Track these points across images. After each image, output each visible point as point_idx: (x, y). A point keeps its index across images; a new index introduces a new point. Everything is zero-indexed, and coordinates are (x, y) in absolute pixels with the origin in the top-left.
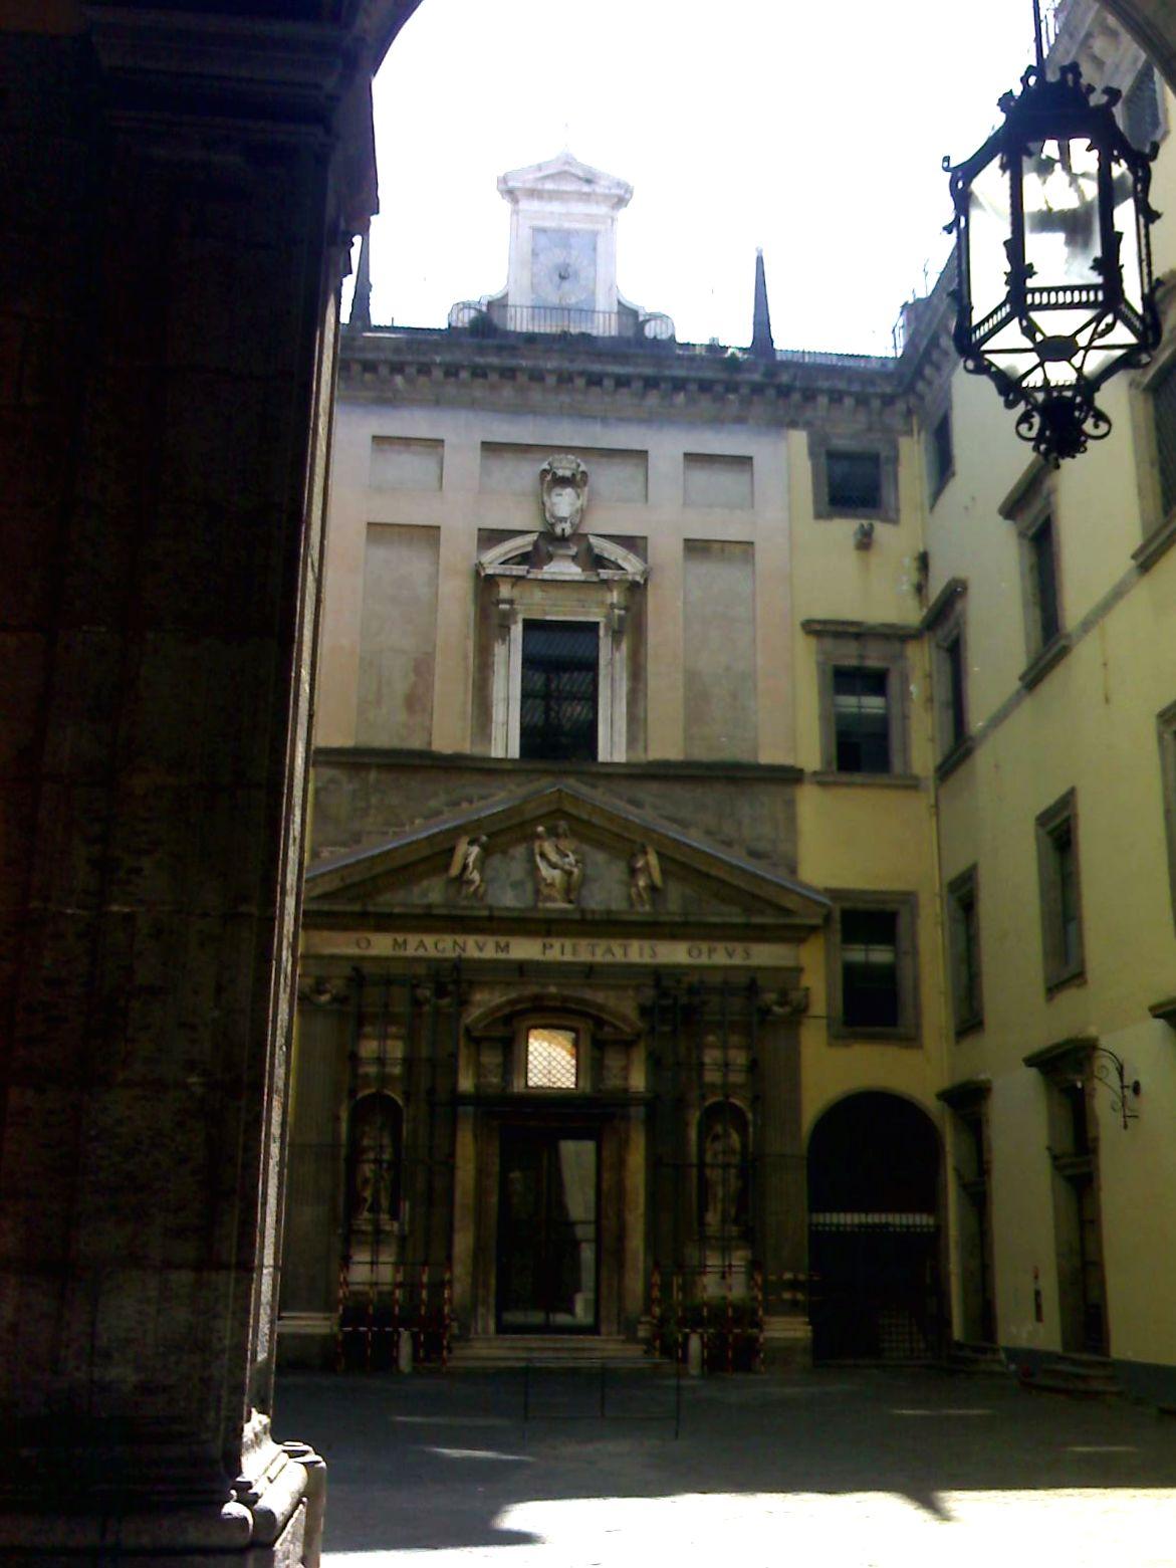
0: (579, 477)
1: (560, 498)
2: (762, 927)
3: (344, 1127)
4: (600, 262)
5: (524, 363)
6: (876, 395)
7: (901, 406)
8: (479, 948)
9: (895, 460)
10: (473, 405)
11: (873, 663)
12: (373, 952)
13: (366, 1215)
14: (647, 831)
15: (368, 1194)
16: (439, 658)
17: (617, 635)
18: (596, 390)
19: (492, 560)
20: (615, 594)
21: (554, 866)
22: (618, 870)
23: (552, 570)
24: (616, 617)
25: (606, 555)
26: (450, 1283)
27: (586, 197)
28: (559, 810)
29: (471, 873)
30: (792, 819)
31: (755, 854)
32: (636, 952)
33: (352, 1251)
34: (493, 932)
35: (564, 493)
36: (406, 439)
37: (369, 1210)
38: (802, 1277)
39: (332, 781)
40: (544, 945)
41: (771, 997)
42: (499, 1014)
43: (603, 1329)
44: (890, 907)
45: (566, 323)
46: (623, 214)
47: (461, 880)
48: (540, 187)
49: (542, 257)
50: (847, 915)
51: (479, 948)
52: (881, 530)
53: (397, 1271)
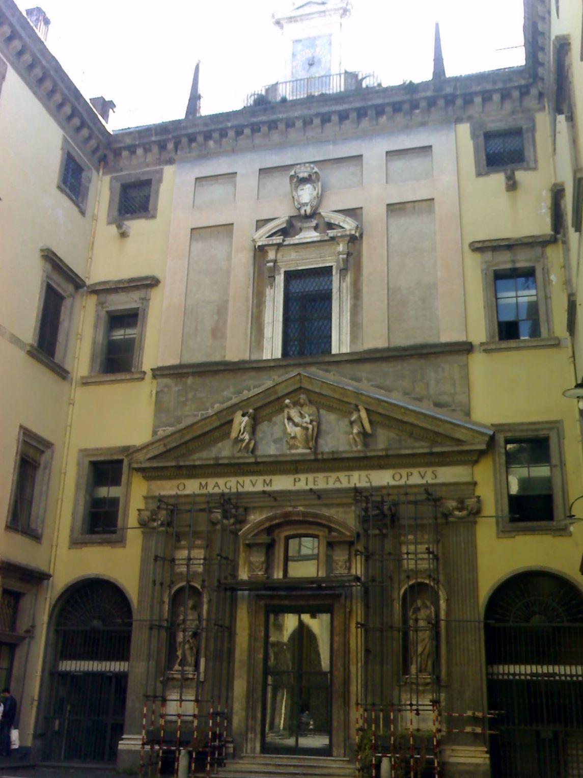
0: (314, 177)
1: (302, 191)
2: (442, 454)
3: (166, 607)
5: (280, 116)
6: (515, 88)
7: (534, 91)
8: (251, 484)
9: (533, 129)
10: (254, 148)
11: (522, 264)
12: (187, 492)
14: (358, 394)
16: (231, 303)
20: (341, 245)
21: (296, 425)
24: (341, 260)
25: (332, 221)
30: (466, 378)
31: (438, 405)
32: (358, 479)
33: (167, 693)
34: (415, 466)
35: (305, 188)
36: (215, 176)
37: (180, 665)
38: (480, 715)
39: (167, 386)
40: (295, 479)
41: (451, 504)
42: (262, 527)
43: (335, 752)
44: (543, 433)
49: (299, 56)
51: (251, 484)
52: (520, 175)
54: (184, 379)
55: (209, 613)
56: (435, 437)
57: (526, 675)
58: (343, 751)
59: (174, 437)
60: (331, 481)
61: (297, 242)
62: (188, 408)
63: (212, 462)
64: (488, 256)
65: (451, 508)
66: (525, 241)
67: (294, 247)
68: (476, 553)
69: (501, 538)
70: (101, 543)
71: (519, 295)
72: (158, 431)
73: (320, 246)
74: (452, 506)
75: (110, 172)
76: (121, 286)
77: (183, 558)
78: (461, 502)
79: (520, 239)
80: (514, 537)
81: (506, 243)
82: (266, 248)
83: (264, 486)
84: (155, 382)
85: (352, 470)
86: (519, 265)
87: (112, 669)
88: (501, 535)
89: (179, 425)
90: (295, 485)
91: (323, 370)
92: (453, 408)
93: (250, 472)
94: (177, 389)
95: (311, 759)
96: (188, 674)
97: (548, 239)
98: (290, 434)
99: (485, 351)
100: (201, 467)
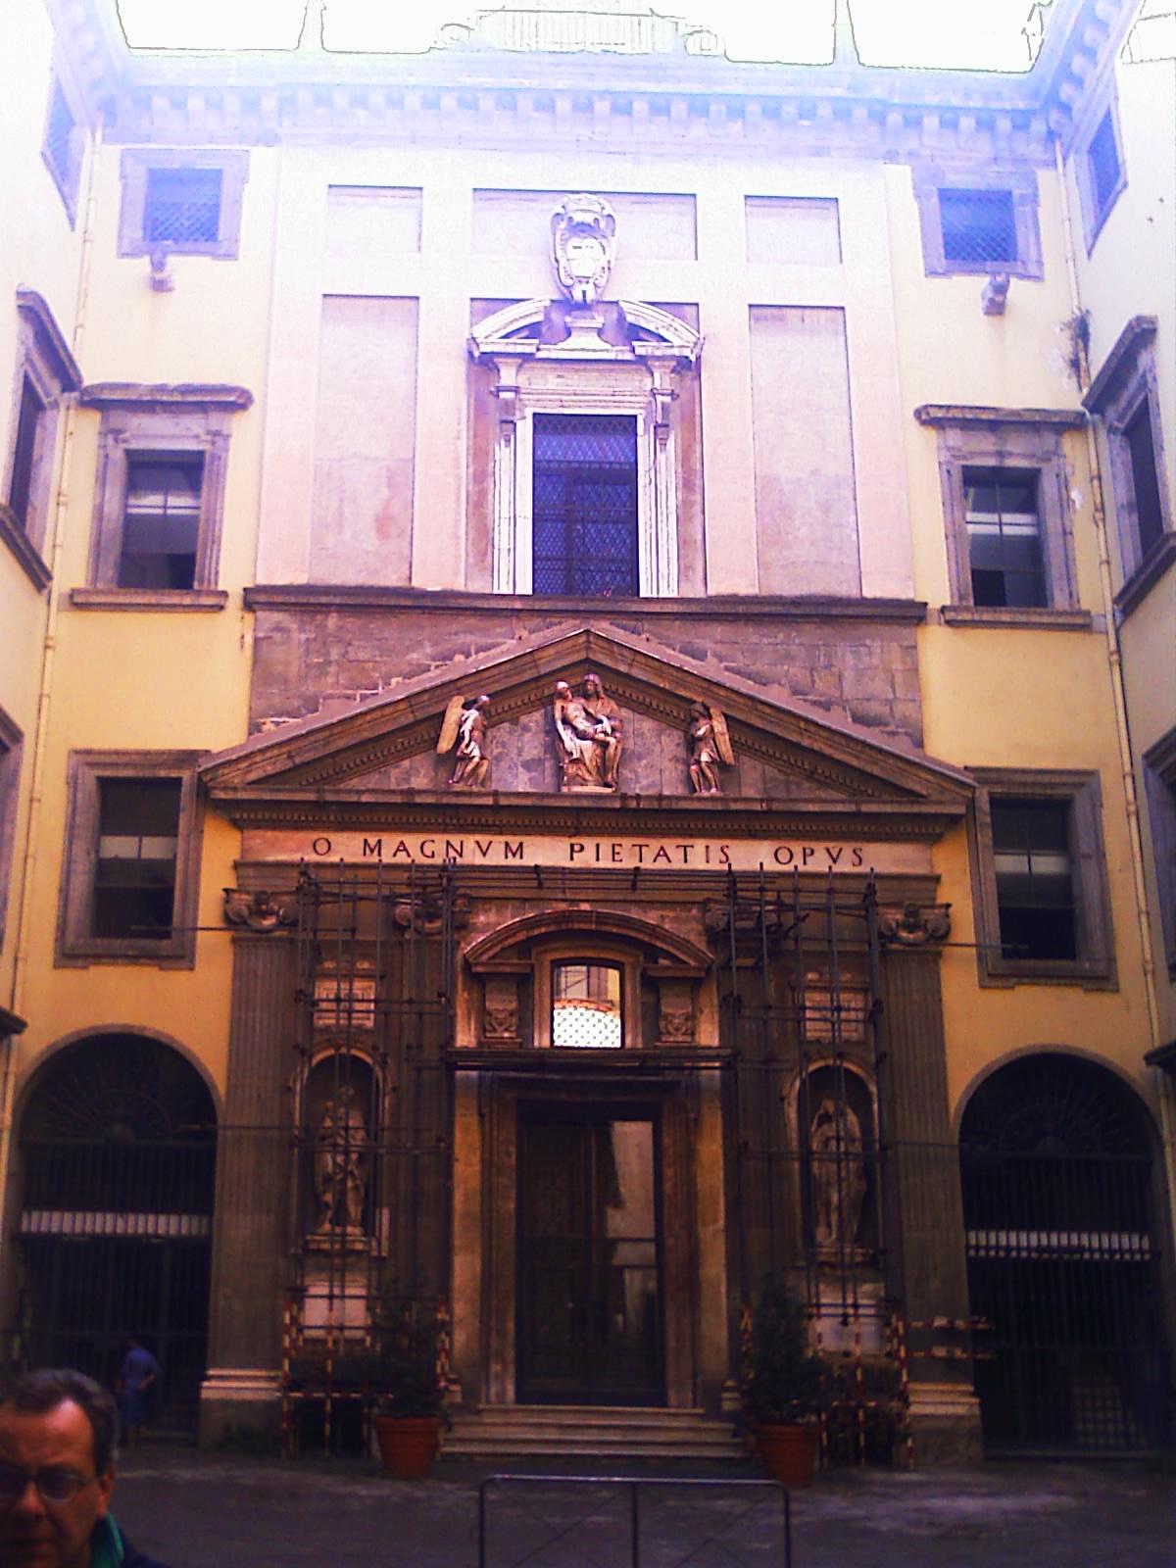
0: (602, 224)
9: (1034, 199)
21: (581, 735)
22: (671, 742)
29: (467, 746)
32: (701, 856)
34: (499, 830)
39: (278, 629)
40: (572, 846)
42: (511, 941)
47: (455, 757)
55: (396, 1115)
56: (860, 782)
57: (1029, 1249)
58: (690, 1396)
59: (312, 738)
60: (648, 854)
62: (330, 680)
63: (398, 799)
64: (954, 437)
65: (894, 925)
66: (1027, 417)
69: (989, 988)
71: (169, 504)
74: (897, 921)
75: (117, 140)
76: (165, 398)
78: (912, 912)
79: (1017, 413)
80: (1012, 988)
81: (992, 416)
82: (496, 360)
83: (506, 857)
84: (249, 617)
85: (691, 836)
86: (1010, 462)
87: (161, 1231)
88: (988, 982)
89: (310, 716)
90: (572, 858)
91: (625, 628)
94: (303, 637)
95: (641, 1413)
96: (354, 1241)
97: (1071, 419)
98: (572, 754)
99: (948, 623)
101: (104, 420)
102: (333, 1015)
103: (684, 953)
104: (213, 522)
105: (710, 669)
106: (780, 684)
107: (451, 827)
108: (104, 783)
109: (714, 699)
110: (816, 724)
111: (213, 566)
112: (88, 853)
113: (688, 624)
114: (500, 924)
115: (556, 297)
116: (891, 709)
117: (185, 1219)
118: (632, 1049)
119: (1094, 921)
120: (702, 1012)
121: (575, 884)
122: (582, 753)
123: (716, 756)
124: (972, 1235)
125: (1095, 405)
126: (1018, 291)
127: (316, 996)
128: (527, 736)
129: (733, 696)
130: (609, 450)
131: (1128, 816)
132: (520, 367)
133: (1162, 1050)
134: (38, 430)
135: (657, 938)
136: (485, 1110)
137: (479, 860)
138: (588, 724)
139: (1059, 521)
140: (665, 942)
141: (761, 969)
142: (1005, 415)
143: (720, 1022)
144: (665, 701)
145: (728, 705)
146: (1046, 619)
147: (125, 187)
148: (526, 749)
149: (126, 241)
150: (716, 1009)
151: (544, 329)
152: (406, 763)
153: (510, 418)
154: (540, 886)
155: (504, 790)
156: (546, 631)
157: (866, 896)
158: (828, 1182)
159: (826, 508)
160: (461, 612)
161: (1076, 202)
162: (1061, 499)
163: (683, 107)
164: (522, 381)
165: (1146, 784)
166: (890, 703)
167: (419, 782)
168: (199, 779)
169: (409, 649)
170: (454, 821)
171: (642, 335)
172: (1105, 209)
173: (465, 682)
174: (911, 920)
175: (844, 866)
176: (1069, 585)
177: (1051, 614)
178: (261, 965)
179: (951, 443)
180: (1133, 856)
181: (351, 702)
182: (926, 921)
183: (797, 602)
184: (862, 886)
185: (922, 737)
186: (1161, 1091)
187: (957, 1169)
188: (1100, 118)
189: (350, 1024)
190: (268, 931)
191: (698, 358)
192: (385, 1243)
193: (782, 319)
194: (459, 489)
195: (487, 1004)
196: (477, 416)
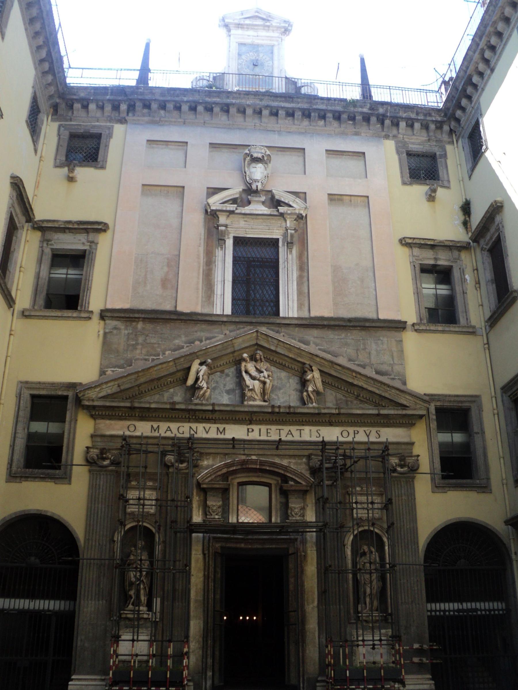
0: (265, 158)
2: (386, 416)
3: (118, 547)
4: (276, 58)
5: (234, 101)
9: (445, 156)
13: (131, 607)
15: (132, 593)
17: (290, 245)
18: (273, 118)
19: (215, 202)
21: (253, 378)
22: (293, 383)
23: (251, 208)
25: (283, 200)
26: (187, 653)
27: (267, 28)
28: (257, 344)
29: (201, 382)
34: (214, 421)
37: (133, 604)
39: (115, 328)
40: (248, 429)
42: (220, 473)
45: (257, 87)
46: (288, 39)
47: (195, 388)
48: (242, 22)
49: (243, 57)
50: (439, 411)
53: (151, 646)
54: (134, 324)
59: (129, 378)
61: (248, 212)
62: (138, 351)
63: (168, 406)
64: (416, 251)
65: (394, 465)
66: (447, 243)
67: (243, 216)
68: (414, 505)
70: (43, 479)
72: (107, 371)
73: (268, 219)
76: (71, 226)
77: (134, 498)
78: (402, 458)
81: (432, 243)
84: (102, 322)
85: (303, 425)
86: (440, 263)
89: (128, 368)
90: (248, 435)
91: (273, 330)
92: (392, 377)
93: (205, 419)
94: (126, 332)
100: (156, 409)
101: (43, 235)
102: (137, 507)
103: (299, 478)
104: (88, 279)
105: (312, 349)
106: (343, 356)
107: (192, 420)
108: (33, 397)
109: (314, 362)
110: (360, 374)
111: (87, 300)
112: (24, 429)
113: (302, 329)
114: (214, 466)
115: (245, 188)
116: (392, 368)
117: (63, 602)
118: (275, 523)
119: (480, 461)
120: (307, 506)
121: (250, 446)
122: (254, 386)
123: (315, 388)
124: (429, 605)
125: (475, 239)
126: (440, 192)
127: (128, 497)
128: (228, 379)
129: (323, 361)
130: (265, 253)
131: (494, 415)
132: (228, 216)
133: (513, 518)
134: (14, 238)
135: (288, 472)
136: (206, 552)
137: (205, 436)
138: (257, 373)
139: (461, 289)
140: (291, 473)
141: (336, 487)
142: (438, 243)
143: (316, 510)
144: (292, 363)
145: (321, 365)
146: (457, 329)
147: (59, 139)
148: (227, 385)
149: (58, 161)
150: (314, 505)
151: (239, 201)
152: (172, 390)
153: (223, 238)
154: (234, 447)
155: (217, 403)
156: (238, 331)
157: (383, 451)
158: (365, 583)
159: (362, 281)
160: (199, 322)
161: (463, 158)
162: (461, 278)
163: (300, 113)
164: (228, 222)
165: (503, 401)
166: (392, 365)
167: (178, 398)
168: (77, 395)
169: (174, 338)
170: (194, 417)
171: (282, 204)
172: (476, 161)
173: (200, 353)
174: (402, 463)
175: (373, 438)
176: (466, 315)
177: (459, 327)
178: (102, 483)
179: (415, 254)
180: (497, 433)
181: (147, 362)
182: (409, 463)
183: (350, 320)
184: (382, 447)
185: (405, 380)
186: (511, 537)
187: (423, 574)
188: (473, 123)
189: (143, 511)
190: (106, 466)
191: (306, 215)
192: (158, 615)
193: (341, 200)
194: (199, 267)
195: (208, 502)
196: (208, 238)
